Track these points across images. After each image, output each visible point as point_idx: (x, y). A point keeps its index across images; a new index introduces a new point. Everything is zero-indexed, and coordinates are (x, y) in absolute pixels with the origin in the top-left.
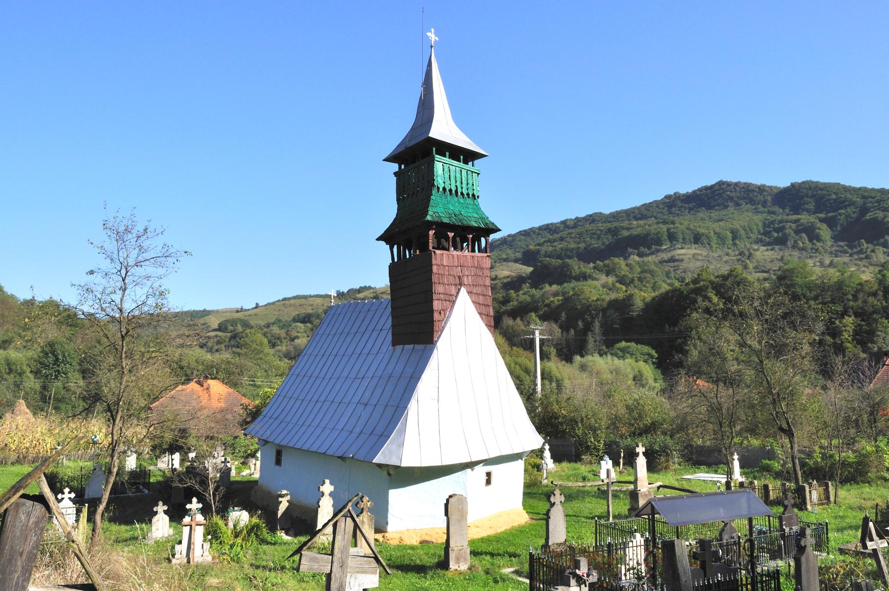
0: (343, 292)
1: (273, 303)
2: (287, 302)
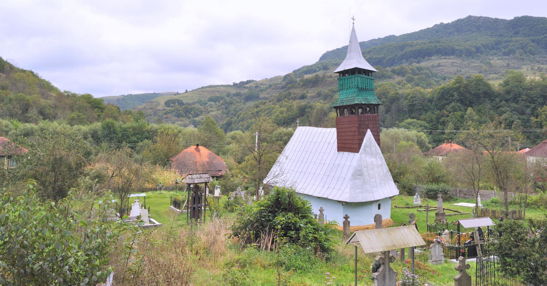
0: (237, 84)
1: (196, 90)
2: (204, 89)
